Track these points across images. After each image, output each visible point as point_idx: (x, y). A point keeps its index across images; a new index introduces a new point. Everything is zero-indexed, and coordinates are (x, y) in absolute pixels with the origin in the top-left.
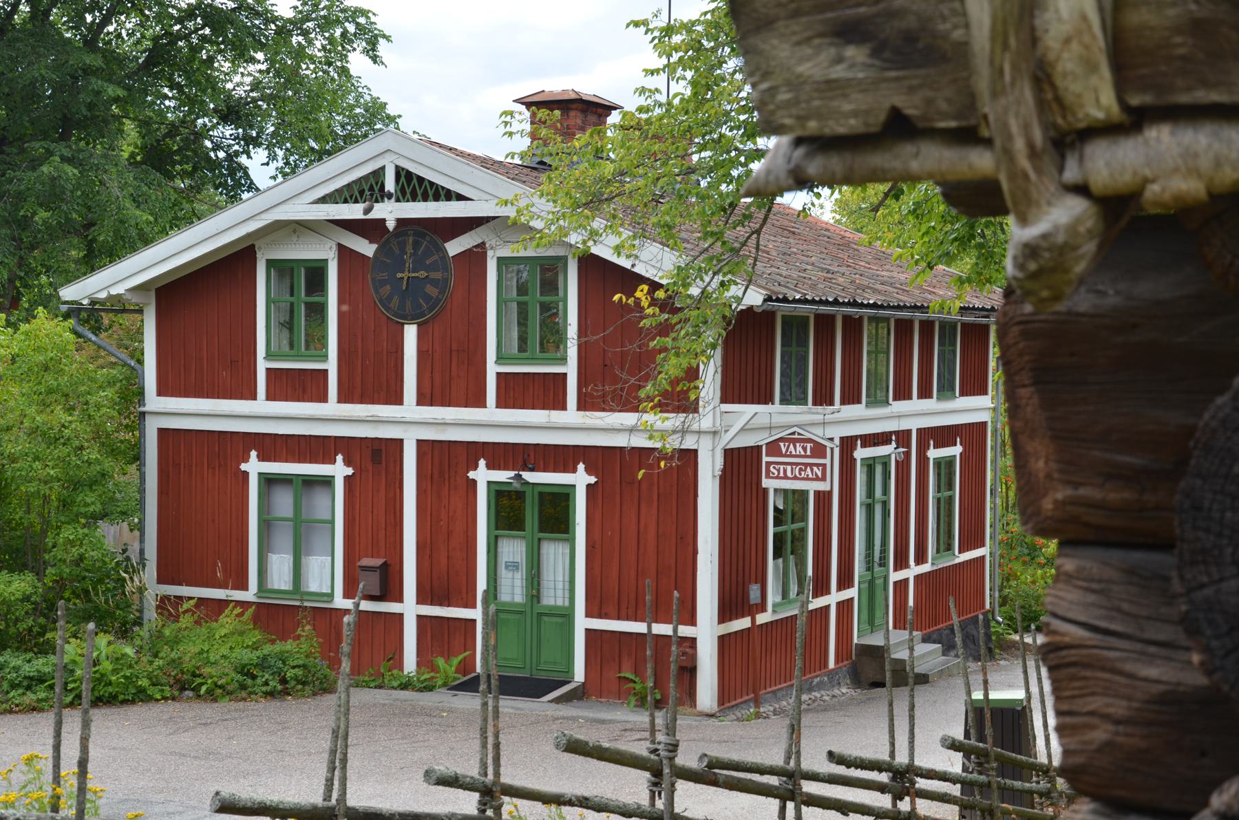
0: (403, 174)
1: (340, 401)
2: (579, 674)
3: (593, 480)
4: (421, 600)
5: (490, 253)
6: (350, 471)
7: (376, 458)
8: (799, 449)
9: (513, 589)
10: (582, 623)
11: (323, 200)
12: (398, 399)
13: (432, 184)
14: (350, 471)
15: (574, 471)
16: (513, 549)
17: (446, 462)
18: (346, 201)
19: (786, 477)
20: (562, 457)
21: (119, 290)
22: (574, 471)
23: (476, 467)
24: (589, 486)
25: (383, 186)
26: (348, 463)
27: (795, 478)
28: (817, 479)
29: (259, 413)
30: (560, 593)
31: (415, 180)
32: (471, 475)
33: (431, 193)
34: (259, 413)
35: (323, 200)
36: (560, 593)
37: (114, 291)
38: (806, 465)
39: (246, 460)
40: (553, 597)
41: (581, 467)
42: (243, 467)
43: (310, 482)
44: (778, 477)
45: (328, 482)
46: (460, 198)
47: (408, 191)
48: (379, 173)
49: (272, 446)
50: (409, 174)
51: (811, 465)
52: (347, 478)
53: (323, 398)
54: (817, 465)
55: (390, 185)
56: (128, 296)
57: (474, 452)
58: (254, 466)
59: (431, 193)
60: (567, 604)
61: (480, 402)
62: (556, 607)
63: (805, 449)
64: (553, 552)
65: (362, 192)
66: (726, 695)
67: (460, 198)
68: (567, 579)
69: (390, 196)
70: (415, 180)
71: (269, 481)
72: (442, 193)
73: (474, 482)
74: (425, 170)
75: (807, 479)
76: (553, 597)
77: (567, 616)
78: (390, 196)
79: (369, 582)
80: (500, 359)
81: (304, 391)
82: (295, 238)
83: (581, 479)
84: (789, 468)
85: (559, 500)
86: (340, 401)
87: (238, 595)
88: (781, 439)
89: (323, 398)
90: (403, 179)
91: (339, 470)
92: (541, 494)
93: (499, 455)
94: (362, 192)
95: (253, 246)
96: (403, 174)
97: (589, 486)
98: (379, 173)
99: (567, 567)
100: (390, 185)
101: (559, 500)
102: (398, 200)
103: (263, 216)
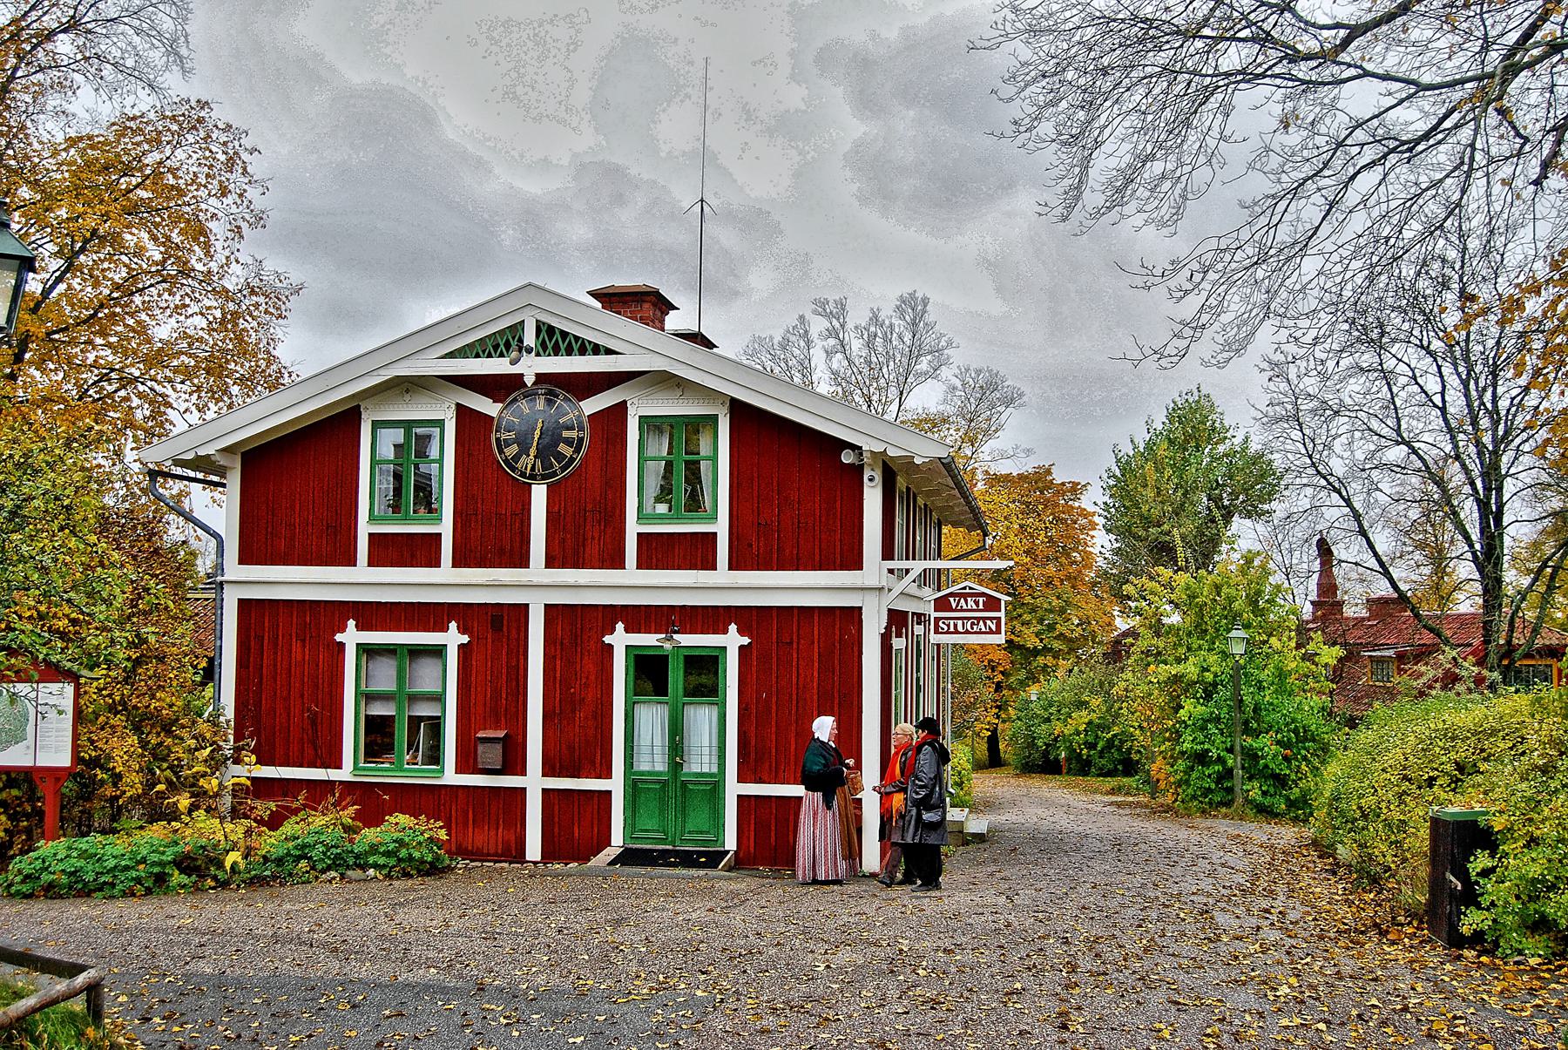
0: (544, 329)
1: (732, 566)
2: (731, 843)
3: (746, 641)
4: (549, 770)
5: (631, 411)
6: (465, 639)
7: (496, 628)
8: (971, 603)
9: (653, 760)
10: (734, 789)
11: (451, 355)
12: (523, 561)
13: (577, 338)
14: (465, 639)
15: (725, 632)
16: (652, 718)
17: (577, 629)
18: (477, 356)
19: (956, 632)
20: (713, 618)
21: (209, 450)
22: (725, 632)
23: (612, 631)
24: (741, 647)
25: (521, 340)
26: (462, 630)
27: (967, 632)
28: (991, 632)
29: (361, 580)
30: (706, 759)
31: (558, 335)
32: (607, 639)
33: (576, 347)
34: (361, 580)
35: (451, 355)
36: (658, 758)
37: (202, 452)
38: (979, 619)
39: (343, 629)
40: (700, 762)
41: (453, 625)
42: (339, 637)
43: (416, 652)
44: (948, 632)
45: (438, 652)
46: (609, 352)
47: (550, 346)
48: (517, 328)
49: (371, 615)
50: (551, 330)
51: (984, 619)
52: (461, 647)
53: (435, 563)
54: (991, 619)
55: (530, 339)
56: (218, 458)
57: (610, 615)
58: (351, 637)
59: (576, 347)
60: (715, 770)
61: (351, 561)
62: (702, 775)
63: (977, 603)
64: (700, 719)
65: (496, 347)
66: (548, 854)
67: (609, 352)
68: (715, 743)
69: (529, 351)
70: (558, 335)
71: (367, 651)
72: (589, 348)
73: (342, 645)
74: (570, 324)
75: (980, 632)
76: (700, 762)
77: (714, 787)
78: (529, 351)
79: (491, 755)
80: (372, 519)
81: (413, 556)
82: (407, 397)
83: (732, 640)
84: (960, 623)
85: (704, 667)
86: (732, 566)
87: (334, 775)
88: (951, 594)
89: (435, 563)
90: (544, 334)
91: (453, 638)
92: (637, 657)
93: (638, 618)
94: (496, 347)
95: (358, 407)
96: (544, 329)
97: (741, 647)
98: (517, 328)
99: (714, 733)
100: (530, 339)
101: (704, 667)
102: (538, 355)
103: (381, 372)
